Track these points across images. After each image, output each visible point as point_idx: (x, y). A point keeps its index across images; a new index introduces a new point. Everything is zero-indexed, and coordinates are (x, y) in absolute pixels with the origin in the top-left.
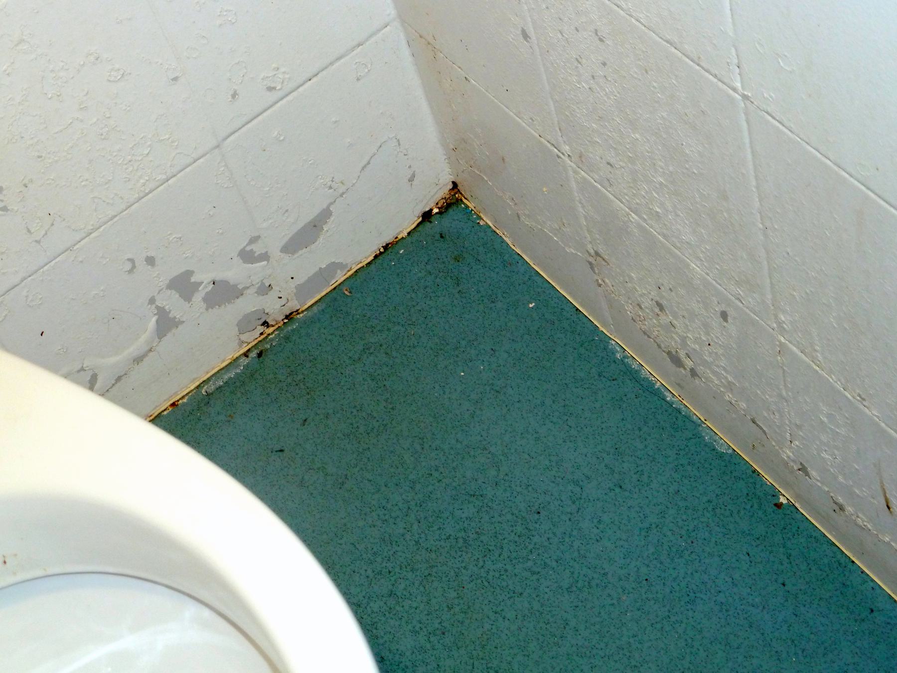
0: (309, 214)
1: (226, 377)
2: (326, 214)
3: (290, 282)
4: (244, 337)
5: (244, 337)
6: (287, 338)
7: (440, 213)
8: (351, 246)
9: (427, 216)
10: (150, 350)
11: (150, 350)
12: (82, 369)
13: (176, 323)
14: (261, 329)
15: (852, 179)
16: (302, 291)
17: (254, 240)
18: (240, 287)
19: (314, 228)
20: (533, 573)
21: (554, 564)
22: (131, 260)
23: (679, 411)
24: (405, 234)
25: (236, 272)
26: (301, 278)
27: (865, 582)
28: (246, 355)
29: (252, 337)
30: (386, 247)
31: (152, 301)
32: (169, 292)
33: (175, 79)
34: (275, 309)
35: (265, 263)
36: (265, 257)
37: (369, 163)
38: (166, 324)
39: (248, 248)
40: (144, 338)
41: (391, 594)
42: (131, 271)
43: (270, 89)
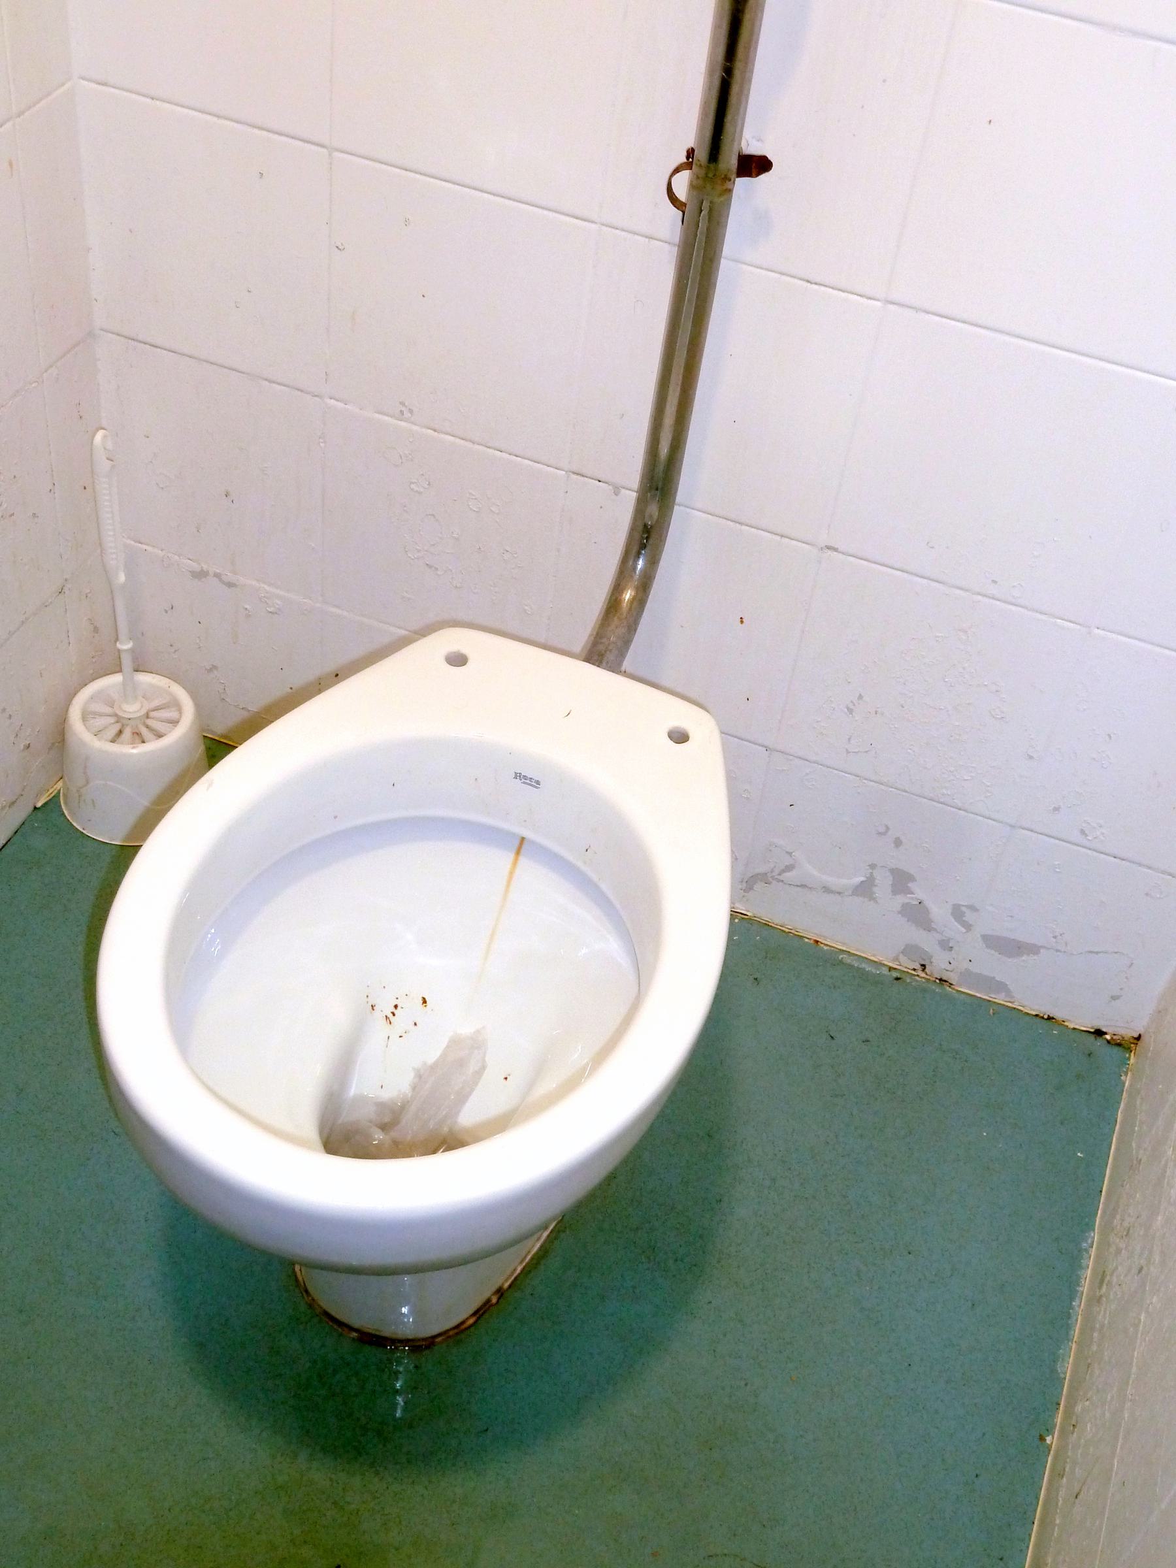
0: (1021, 936)
1: (863, 965)
2: (1034, 949)
3: (967, 962)
4: (902, 958)
5: (902, 958)
6: (924, 990)
7: (1108, 1042)
8: (1029, 988)
9: (1099, 1033)
10: (839, 893)
11: (839, 893)
12: (790, 854)
13: (872, 898)
14: (918, 967)
15: (477, 447)
16: (967, 975)
17: (973, 908)
18: (933, 925)
19: (1013, 948)
20: (858, 1275)
21: (876, 1287)
22: (888, 828)
23: (1069, 1317)
24: (1071, 1026)
25: (939, 912)
26: (975, 968)
27: (1023, 1540)
28: (890, 969)
29: (907, 964)
30: (1050, 1018)
31: (873, 866)
32: (888, 874)
33: (1031, 757)
34: (940, 964)
35: (964, 930)
36: (968, 927)
37: (1097, 953)
38: (865, 889)
39: (964, 909)
40: (845, 881)
41: (774, 1180)
42: (880, 834)
43: (1083, 832)
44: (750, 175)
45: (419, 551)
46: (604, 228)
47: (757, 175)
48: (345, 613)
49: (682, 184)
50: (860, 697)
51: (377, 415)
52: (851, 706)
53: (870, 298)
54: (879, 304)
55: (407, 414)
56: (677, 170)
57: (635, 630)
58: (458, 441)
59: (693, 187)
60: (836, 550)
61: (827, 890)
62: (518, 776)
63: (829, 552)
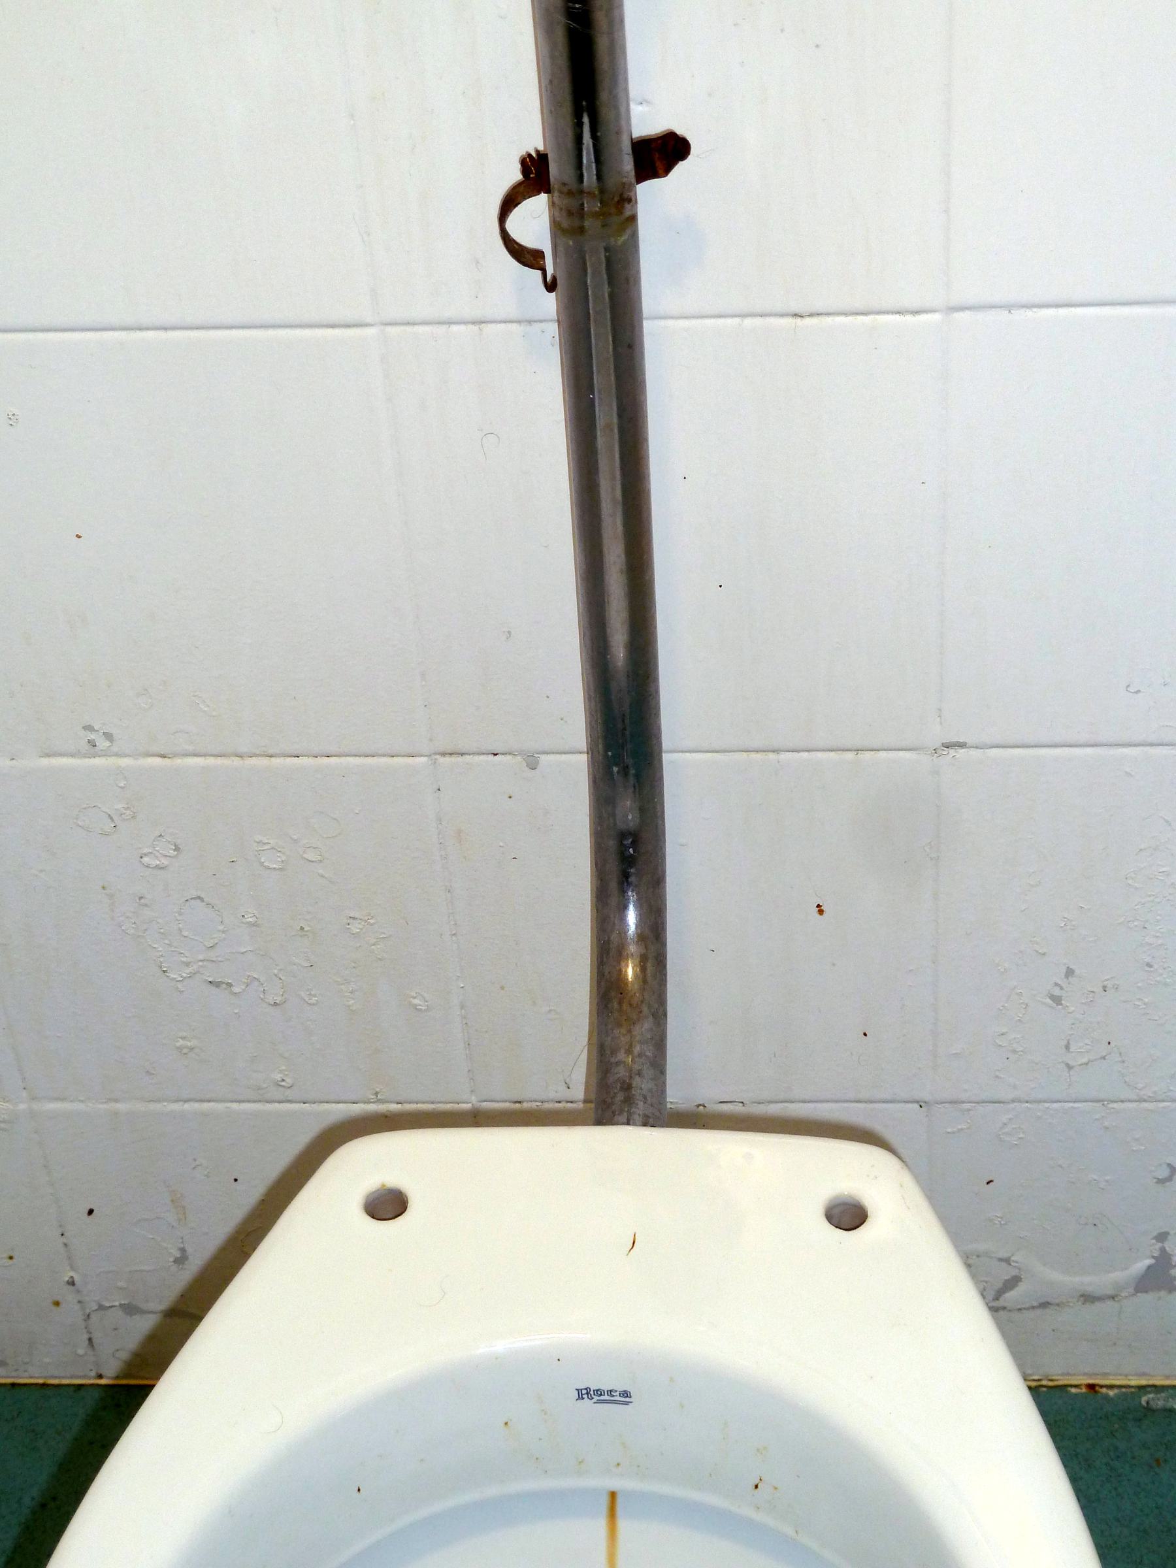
12: (1007, 1261)
31: (1162, 1237)
40: (1117, 1276)
42: (1161, 1181)
44: (656, 175)
45: (188, 964)
46: (389, 329)
47: (667, 171)
48: (80, 1106)
49: (534, 221)
50: (1070, 972)
51: (45, 761)
52: (1057, 992)
53: (916, 312)
54: (937, 317)
55: (103, 744)
56: (509, 203)
57: (665, 1015)
58: (211, 761)
59: (557, 229)
60: (962, 745)
61: (1088, 1298)
62: (584, 1394)
63: (952, 752)
